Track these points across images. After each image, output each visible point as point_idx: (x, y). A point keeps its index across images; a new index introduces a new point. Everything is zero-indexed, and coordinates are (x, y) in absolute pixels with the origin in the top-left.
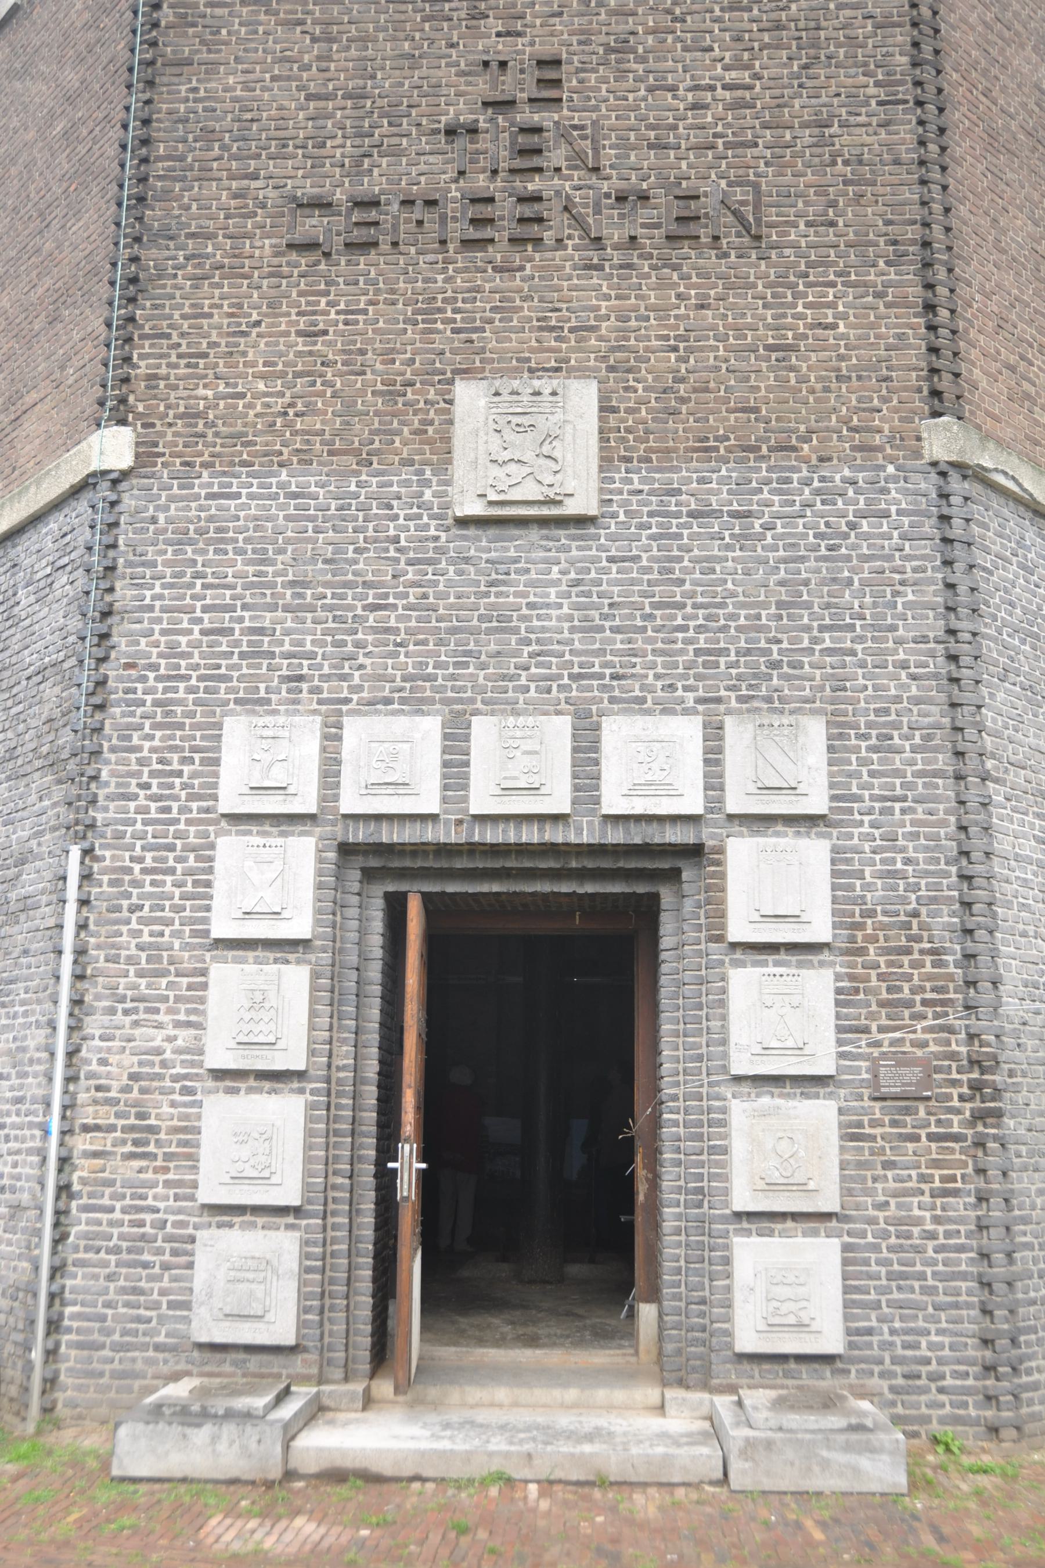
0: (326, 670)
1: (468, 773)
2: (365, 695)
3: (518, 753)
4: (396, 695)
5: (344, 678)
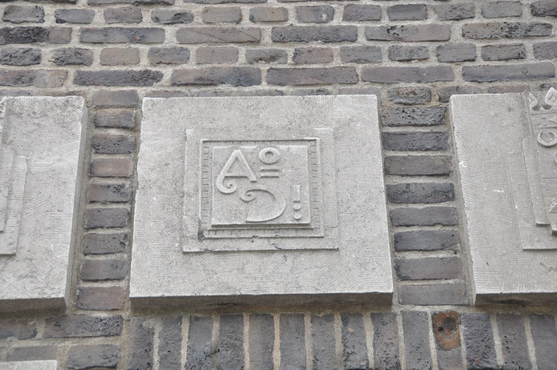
0: (99, 20)
2: (191, 66)
4: (264, 67)
5: (138, 36)
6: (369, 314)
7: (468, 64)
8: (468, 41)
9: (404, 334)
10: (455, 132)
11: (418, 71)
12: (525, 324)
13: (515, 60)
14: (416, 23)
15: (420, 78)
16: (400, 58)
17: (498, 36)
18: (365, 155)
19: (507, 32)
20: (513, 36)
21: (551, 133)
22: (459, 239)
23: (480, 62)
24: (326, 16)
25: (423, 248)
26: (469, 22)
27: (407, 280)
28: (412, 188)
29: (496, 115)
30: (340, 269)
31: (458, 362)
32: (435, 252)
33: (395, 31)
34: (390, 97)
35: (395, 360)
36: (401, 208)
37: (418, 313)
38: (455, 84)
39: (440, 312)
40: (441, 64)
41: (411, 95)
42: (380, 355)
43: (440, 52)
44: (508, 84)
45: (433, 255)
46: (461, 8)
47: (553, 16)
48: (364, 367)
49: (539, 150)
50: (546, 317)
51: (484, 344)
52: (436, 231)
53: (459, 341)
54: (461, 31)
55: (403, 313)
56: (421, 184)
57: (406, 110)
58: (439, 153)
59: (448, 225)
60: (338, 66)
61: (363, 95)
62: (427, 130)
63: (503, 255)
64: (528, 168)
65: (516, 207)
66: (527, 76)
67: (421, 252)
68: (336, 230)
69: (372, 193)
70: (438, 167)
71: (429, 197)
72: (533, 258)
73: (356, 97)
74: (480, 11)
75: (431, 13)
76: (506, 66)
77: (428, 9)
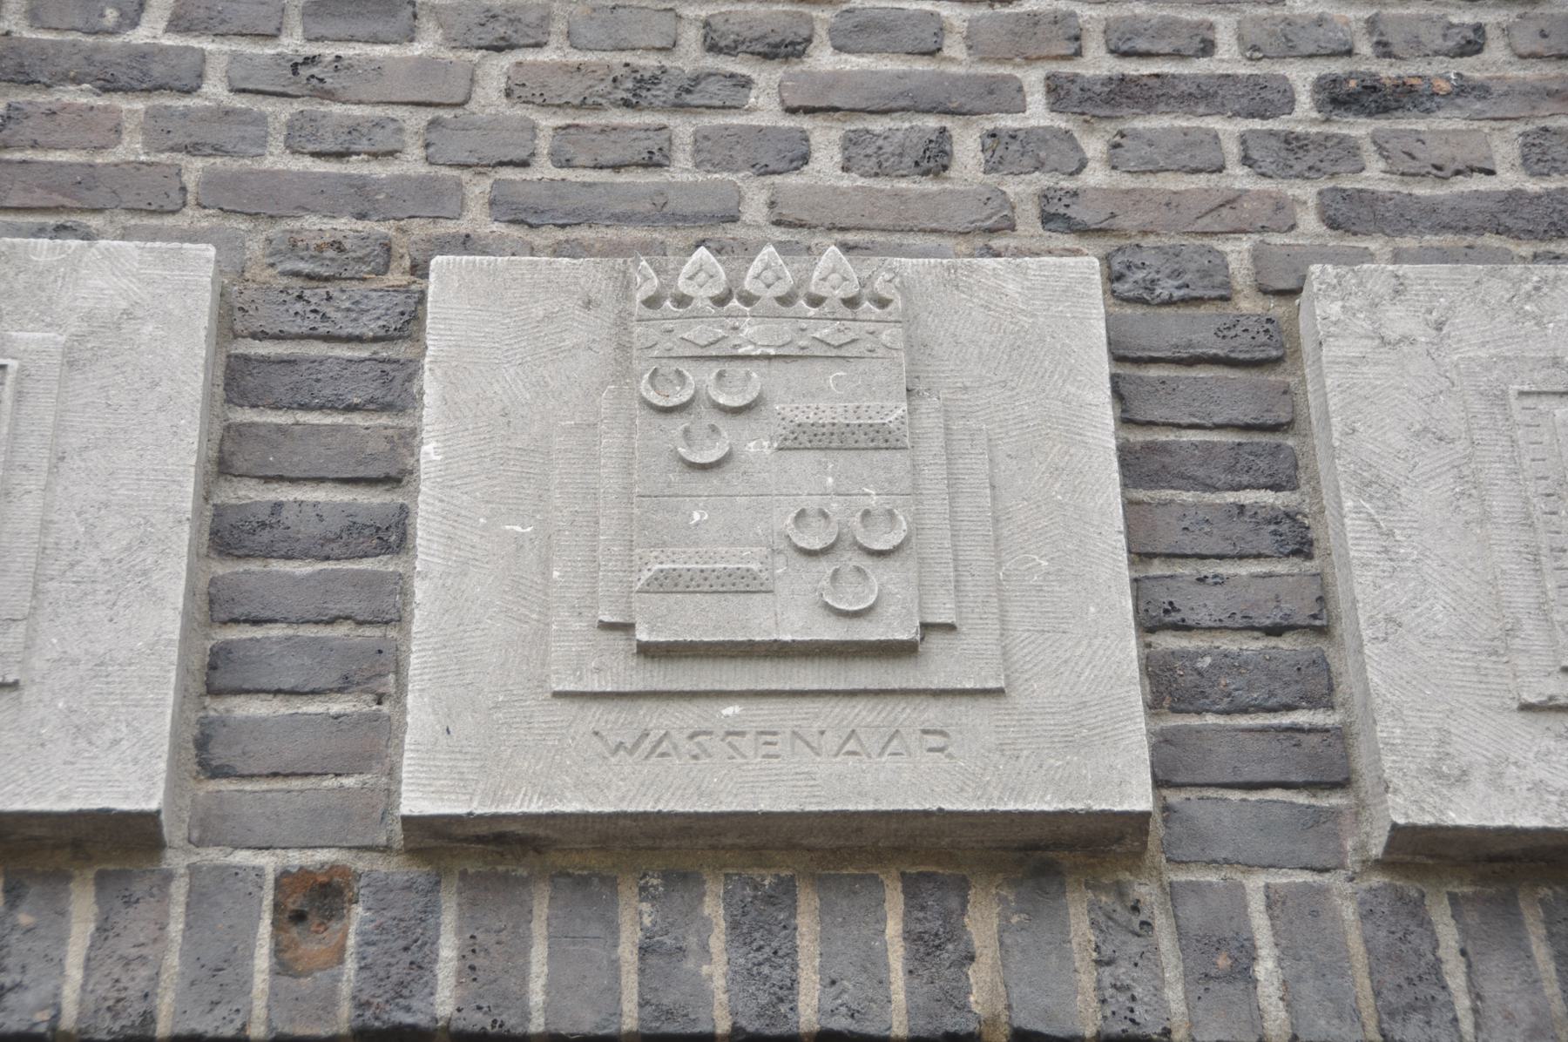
1: (401, 586)
3: (756, 445)
6: (90, 875)
7: (508, 173)
8: (519, 111)
9: (184, 931)
10: (427, 360)
11: (364, 186)
12: (535, 902)
13: (640, 170)
14: (380, 51)
15: (367, 206)
16: (318, 148)
17: (603, 101)
18: (151, 415)
19: (627, 90)
20: (643, 103)
21: (679, 373)
22: (397, 662)
23: (544, 170)
24: (116, 14)
25: (286, 687)
26: (529, 56)
27: (227, 776)
28: (288, 516)
29: (549, 317)
30: (13, 741)
31: (324, 1009)
32: (322, 698)
33: (315, 71)
34: (271, 255)
35: (140, 1007)
36: (246, 572)
37: (236, 872)
38: (462, 226)
39: (301, 868)
40: (434, 169)
41: (330, 253)
42: (101, 991)
43: (433, 137)
44: (611, 234)
45: (314, 707)
46: (512, 16)
47: (759, 54)
48: (42, 1029)
49: (641, 416)
50: (596, 880)
51: (407, 958)
52: (335, 639)
53: (342, 949)
54: (504, 80)
55: (193, 870)
56: (315, 505)
57: (307, 293)
58: (384, 420)
59: (371, 623)
60: (132, 158)
61: (175, 245)
62: (363, 352)
63: (497, 707)
64: (605, 466)
65: (556, 574)
66: (664, 216)
67: (280, 697)
68: (21, 628)
69: (152, 526)
70: (374, 457)
71: (333, 541)
72: (575, 718)
73: (152, 250)
74: (563, 27)
75: (428, 25)
76: (612, 184)
77: (420, 13)
